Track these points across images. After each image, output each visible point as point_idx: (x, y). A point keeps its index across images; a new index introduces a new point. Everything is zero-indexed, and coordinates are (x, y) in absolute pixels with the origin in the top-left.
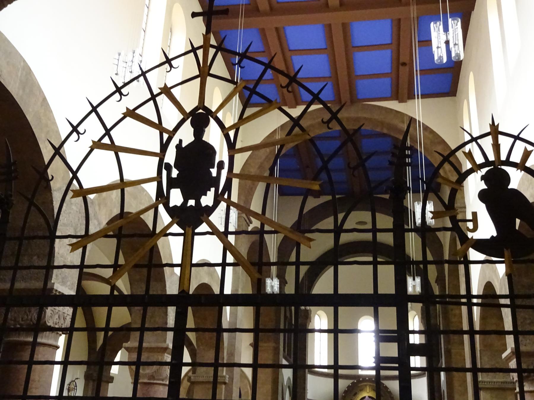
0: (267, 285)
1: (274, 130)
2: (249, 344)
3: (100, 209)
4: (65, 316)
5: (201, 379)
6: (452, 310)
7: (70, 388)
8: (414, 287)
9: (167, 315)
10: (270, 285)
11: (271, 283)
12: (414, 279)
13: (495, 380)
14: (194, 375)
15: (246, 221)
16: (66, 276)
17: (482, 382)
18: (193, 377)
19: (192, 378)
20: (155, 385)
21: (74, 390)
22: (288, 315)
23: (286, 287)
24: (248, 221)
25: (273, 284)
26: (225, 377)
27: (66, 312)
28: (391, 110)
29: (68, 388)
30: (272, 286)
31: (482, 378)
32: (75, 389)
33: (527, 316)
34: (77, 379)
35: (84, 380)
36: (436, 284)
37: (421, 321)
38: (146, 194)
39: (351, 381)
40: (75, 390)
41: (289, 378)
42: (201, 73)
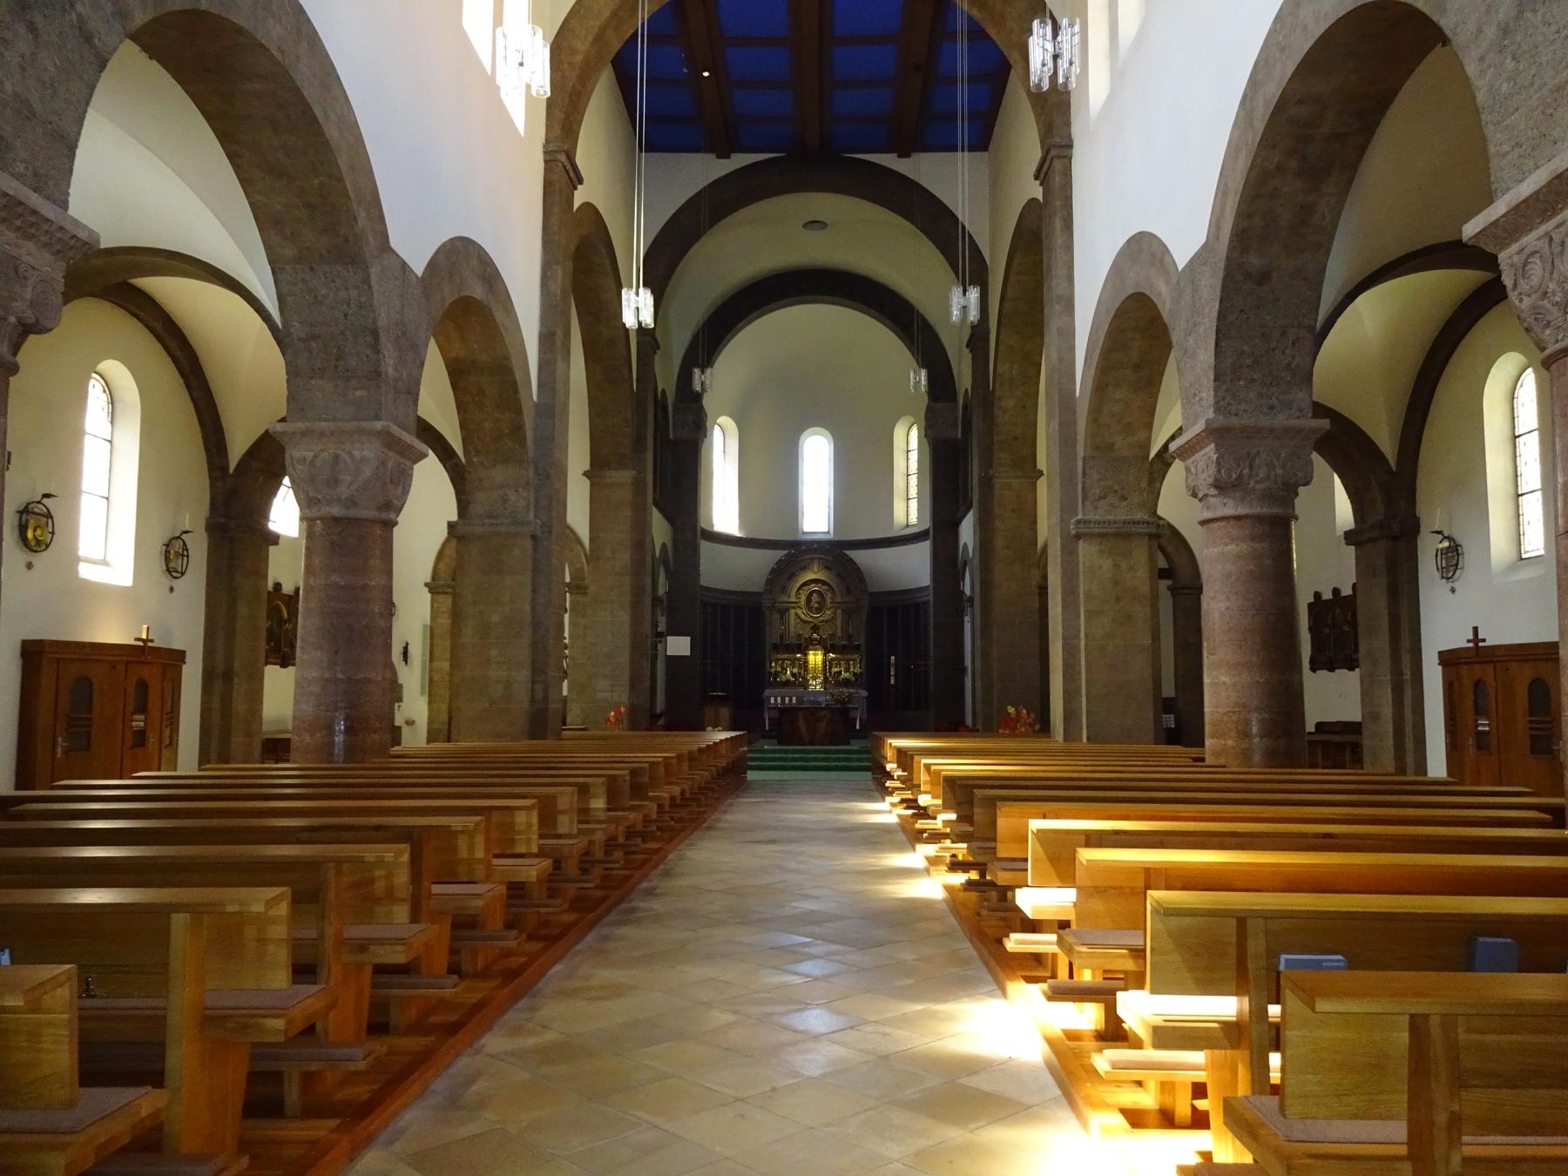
15: (567, 172)
24: (572, 175)
31: (1084, 514)
33: (1246, 348)
34: (186, 532)
40: (185, 558)
41: (664, 545)
42: (476, 509)
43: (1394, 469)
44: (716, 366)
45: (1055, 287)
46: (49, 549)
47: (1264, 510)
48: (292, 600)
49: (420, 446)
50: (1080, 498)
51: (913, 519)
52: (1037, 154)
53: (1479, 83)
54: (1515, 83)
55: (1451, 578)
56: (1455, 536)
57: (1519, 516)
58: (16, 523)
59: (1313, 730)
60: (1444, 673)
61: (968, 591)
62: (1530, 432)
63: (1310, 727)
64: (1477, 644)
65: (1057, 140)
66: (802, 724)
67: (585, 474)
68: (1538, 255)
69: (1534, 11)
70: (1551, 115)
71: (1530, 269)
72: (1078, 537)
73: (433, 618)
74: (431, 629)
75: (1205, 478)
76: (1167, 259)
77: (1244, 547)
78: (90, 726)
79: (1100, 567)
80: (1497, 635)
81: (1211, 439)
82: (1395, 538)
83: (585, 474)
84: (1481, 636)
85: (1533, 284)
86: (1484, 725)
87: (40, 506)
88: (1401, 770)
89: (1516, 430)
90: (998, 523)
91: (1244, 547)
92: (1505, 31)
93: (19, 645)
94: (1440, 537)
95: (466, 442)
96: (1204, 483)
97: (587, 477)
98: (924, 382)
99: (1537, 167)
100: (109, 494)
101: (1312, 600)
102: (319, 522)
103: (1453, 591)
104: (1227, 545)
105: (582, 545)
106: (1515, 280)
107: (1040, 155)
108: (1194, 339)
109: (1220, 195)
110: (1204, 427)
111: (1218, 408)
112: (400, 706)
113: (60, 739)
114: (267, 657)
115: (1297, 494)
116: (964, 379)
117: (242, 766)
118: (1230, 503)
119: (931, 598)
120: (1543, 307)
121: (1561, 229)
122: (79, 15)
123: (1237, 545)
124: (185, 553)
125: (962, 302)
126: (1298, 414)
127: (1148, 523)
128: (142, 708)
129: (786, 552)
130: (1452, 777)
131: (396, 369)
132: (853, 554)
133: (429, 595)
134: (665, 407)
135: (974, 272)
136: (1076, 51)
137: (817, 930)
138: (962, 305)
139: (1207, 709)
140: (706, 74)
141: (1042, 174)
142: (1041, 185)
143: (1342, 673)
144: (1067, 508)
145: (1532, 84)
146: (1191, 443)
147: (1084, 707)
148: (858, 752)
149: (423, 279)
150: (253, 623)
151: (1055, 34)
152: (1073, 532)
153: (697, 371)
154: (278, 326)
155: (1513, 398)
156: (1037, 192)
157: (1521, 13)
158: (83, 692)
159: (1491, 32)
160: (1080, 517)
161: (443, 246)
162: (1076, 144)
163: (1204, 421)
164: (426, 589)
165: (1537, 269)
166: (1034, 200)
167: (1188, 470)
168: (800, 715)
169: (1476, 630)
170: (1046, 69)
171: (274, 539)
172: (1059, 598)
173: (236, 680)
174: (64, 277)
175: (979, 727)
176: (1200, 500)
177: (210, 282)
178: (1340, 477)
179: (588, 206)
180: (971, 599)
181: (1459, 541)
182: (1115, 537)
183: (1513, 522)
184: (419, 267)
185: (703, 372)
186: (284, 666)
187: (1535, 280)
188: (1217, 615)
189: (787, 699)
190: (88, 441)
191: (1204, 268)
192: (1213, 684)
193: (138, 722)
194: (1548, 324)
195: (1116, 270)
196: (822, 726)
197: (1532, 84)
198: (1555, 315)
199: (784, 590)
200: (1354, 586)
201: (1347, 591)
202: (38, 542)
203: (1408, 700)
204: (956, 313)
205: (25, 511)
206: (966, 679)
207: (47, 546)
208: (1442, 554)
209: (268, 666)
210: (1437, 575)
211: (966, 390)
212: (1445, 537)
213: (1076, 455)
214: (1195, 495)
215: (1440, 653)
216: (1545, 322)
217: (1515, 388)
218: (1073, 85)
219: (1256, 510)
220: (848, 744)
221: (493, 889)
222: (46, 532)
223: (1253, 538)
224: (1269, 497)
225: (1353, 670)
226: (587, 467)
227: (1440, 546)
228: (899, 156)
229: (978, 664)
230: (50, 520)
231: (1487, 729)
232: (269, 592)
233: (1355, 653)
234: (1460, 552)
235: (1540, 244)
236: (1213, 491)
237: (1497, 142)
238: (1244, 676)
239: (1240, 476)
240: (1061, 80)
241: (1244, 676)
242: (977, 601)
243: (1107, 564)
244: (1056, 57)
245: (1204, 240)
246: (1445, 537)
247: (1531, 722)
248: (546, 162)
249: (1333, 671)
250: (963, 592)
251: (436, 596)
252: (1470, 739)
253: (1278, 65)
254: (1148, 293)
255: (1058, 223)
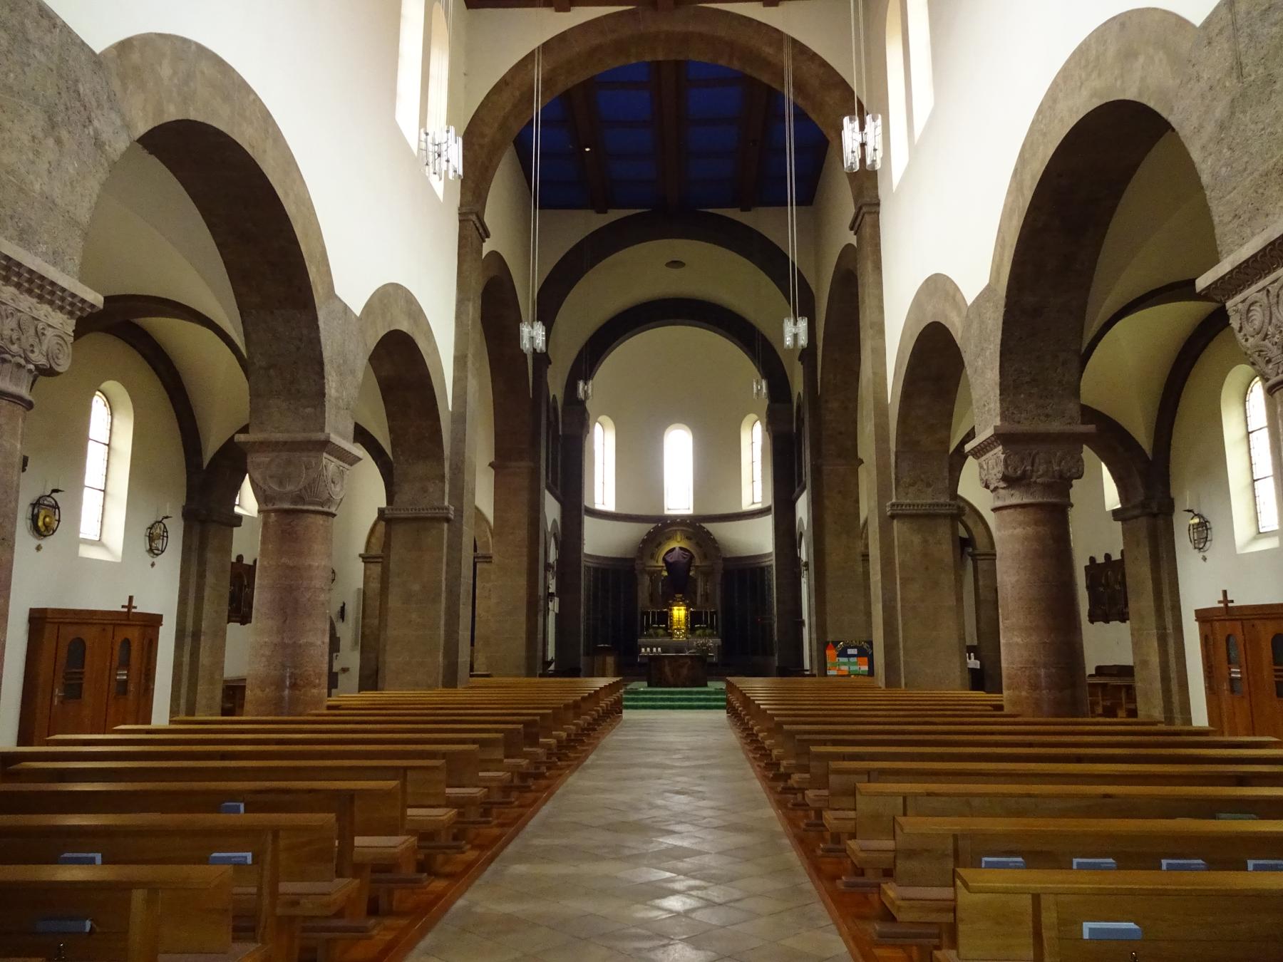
0: (522, 336)
1: (527, 56)
2: (488, 464)
3: (125, 88)
4: (40, 326)
5: (403, 514)
6: (826, 402)
7: (152, 534)
8: (795, 336)
9: (323, 378)
10: (528, 335)
11: (530, 332)
12: (795, 324)
13: (918, 501)
14: (390, 507)
16: (30, 226)
17: (898, 506)
18: (389, 510)
19: (386, 512)
20: (306, 515)
21: (161, 538)
22: (552, 418)
23: (549, 371)
24: (481, 230)
25: (534, 334)
26: (447, 509)
27: (43, 318)
28: (750, 20)
29: (148, 534)
30: (533, 337)
31: (897, 498)
32: (163, 536)
34: (167, 517)
35: (182, 523)
36: (800, 363)
37: (765, 429)
38: (254, 100)
39: (653, 525)
40: (165, 539)
41: (555, 521)
43: (1150, 458)
44: (595, 378)
45: (866, 318)
46: (55, 534)
47: (1045, 499)
48: (251, 569)
49: (358, 450)
50: (894, 486)
51: (758, 498)
52: (851, 211)
53: (1203, 166)
54: (1232, 167)
55: (1202, 548)
56: (1205, 515)
57: (1255, 497)
58: (29, 515)
59: (1094, 673)
60: (1201, 629)
61: (804, 557)
62: (1261, 429)
63: (1090, 670)
64: (1226, 605)
65: (867, 200)
66: (667, 669)
67: (491, 465)
68: (1258, 304)
69: (1244, 112)
70: (1263, 194)
71: (1252, 316)
72: (893, 517)
73: (365, 583)
74: (364, 593)
75: (996, 472)
76: (958, 296)
77: (1030, 530)
78: (81, 679)
79: (912, 542)
80: (1241, 598)
81: (999, 442)
82: (1155, 516)
83: (491, 465)
84: (1229, 598)
85: (1255, 327)
86: (1236, 673)
87: (49, 499)
88: (1169, 720)
89: (1249, 427)
90: (827, 503)
91: (1030, 530)
92: (1222, 127)
93: (28, 611)
94: (1192, 515)
95: (394, 445)
96: (995, 477)
97: (493, 467)
98: (764, 390)
99: (1253, 234)
100: (105, 487)
101: (1088, 564)
102: (273, 514)
103: (1205, 559)
104: (1015, 529)
105: (487, 522)
106: (1241, 324)
107: (854, 211)
108: (982, 360)
109: (999, 248)
110: (993, 433)
111: (1004, 416)
112: (337, 656)
113: (57, 690)
114: (229, 616)
115: (1071, 486)
116: (798, 386)
117: (196, 785)
118: (1016, 493)
119: (774, 563)
120: (1266, 346)
121: (1276, 284)
122: (96, 130)
123: (1024, 528)
124: (165, 534)
125: (793, 330)
126: (1069, 421)
127: (950, 505)
128: (125, 664)
129: (653, 525)
130: (1212, 727)
131: (337, 391)
132: (709, 526)
133: (363, 564)
134: (555, 409)
135: (806, 308)
136: (879, 139)
137: (680, 865)
138: (794, 332)
139: (1004, 664)
140: (588, 150)
141: (856, 226)
142: (855, 234)
143: (1115, 624)
144: (883, 493)
145: (1245, 169)
146: (982, 445)
147: (902, 658)
148: (716, 693)
149: (360, 319)
150: (217, 590)
151: (862, 128)
152: (889, 513)
153: (581, 384)
154: (243, 356)
155: (1246, 401)
156: (852, 239)
157: (1233, 113)
158: (78, 650)
159: (1210, 128)
160: (894, 500)
161: (378, 290)
162: (882, 203)
163: (992, 428)
164: (361, 559)
165: (1258, 315)
166: (849, 246)
167: (981, 467)
168: (667, 662)
169: (1225, 593)
170: (856, 154)
171: (238, 520)
172: (878, 567)
173: (202, 638)
174: (74, 331)
175: (815, 672)
176: (992, 491)
177: (191, 321)
178: (1110, 470)
179: (494, 255)
180: (807, 564)
181: (1208, 518)
182: (920, 518)
183: (1251, 503)
184: (357, 308)
185: (586, 384)
186: (243, 623)
187: (1257, 324)
188: (1009, 587)
189: (655, 650)
190: (91, 445)
191: (988, 304)
192: (1008, 645)
193: (122, 676)
194: (1269, 361)
195: (917, 303)
196: (685, 671)
197: (1245, 169)
198: (1274, 352)
199: (653, 556)
200: (1122, 552)
201: (1116, 556)
202: (46, 526)
203: (1172, 651)
204: (788, 341)
205: (36, 504)
206: (804, 630)
207: (54, 531)
208: (1194, 529)
209: (230, 624)
210: (1191, 546)
211: (799, 394)
212: (1196, 515)
213: (889, 451)
214: (987, 487)
215: (1197, 611)
216: (1267, 358)
217: (1246, 394)
218: (878, 166)
219: (1038, 499)
220: (706, 685)
221: (407, 840)
222: (54, 520)
223: (1036, 523)
224: (1048, 488)
225: (1125, 622)
226: (492, 459)
227: (1192, 522)
228: (742, 210)
229: (814, 619)
230: (57, 510)
231: (1239, 676)
232: (233, 563)
233: (1125, 607)
234: (1208, 527)
235: (1259, 295)
236: (1002, 484)
237: (1219, 211)
238: (1033, 638)
239: (1024, 471)
240: (868, 162)
241: (1033, 638)
242: (812, 567)
243: (917, 539)
244: (863, 145)
245: (988, 282)
246: (1196, 515)
247: (1276, 670)
248: (460, 221)
249: (1108, 623)
250: (800, 558)
251: (369, 565)
252: (1225, 684)
253: (1041, 148)
254: (943, 322)
255: (869, 266)
